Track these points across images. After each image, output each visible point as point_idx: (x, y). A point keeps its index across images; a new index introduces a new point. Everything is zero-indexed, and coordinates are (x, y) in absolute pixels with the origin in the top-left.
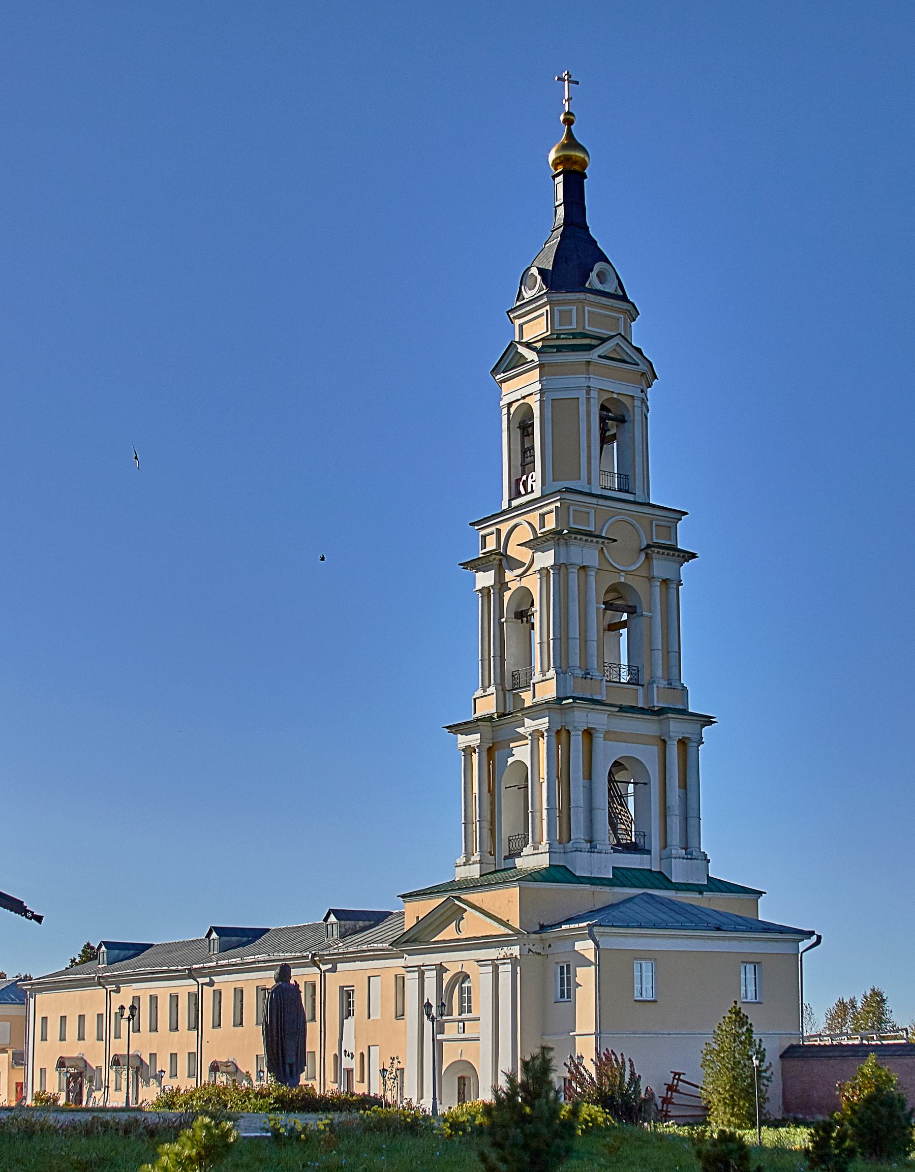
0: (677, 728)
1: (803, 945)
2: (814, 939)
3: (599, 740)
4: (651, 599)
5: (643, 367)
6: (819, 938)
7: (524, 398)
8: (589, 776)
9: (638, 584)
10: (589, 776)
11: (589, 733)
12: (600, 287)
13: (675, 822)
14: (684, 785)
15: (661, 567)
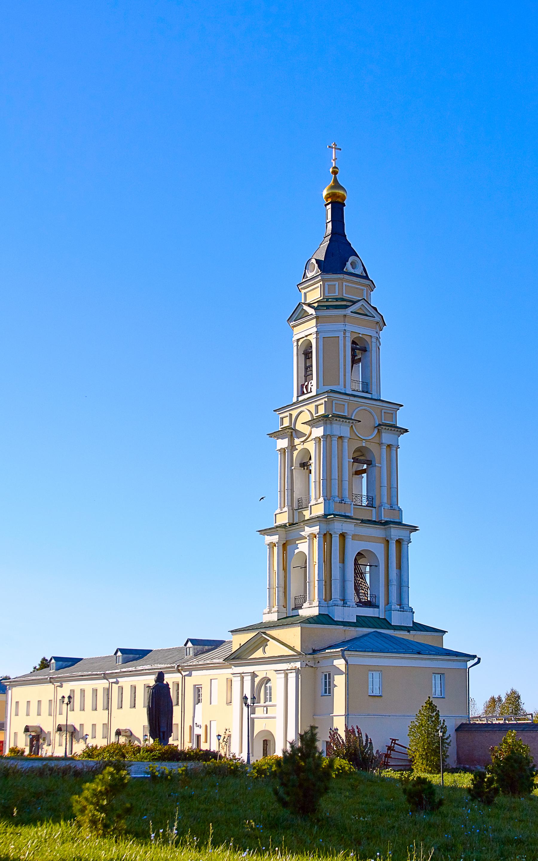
0: (395, 533)
1: (470, 663)
2: (476, 660)
3: (349, 541)
4: (380, 456)
5: (377, 319)
6: (479, 659)
7: (306, 336)
8: (343, 561)
9: (373, 448)
10: (343, 561)
11: (343, 536)
12: (352, 271)
13: (394, 590)
14: (399, 567)
15: (387, 437)
